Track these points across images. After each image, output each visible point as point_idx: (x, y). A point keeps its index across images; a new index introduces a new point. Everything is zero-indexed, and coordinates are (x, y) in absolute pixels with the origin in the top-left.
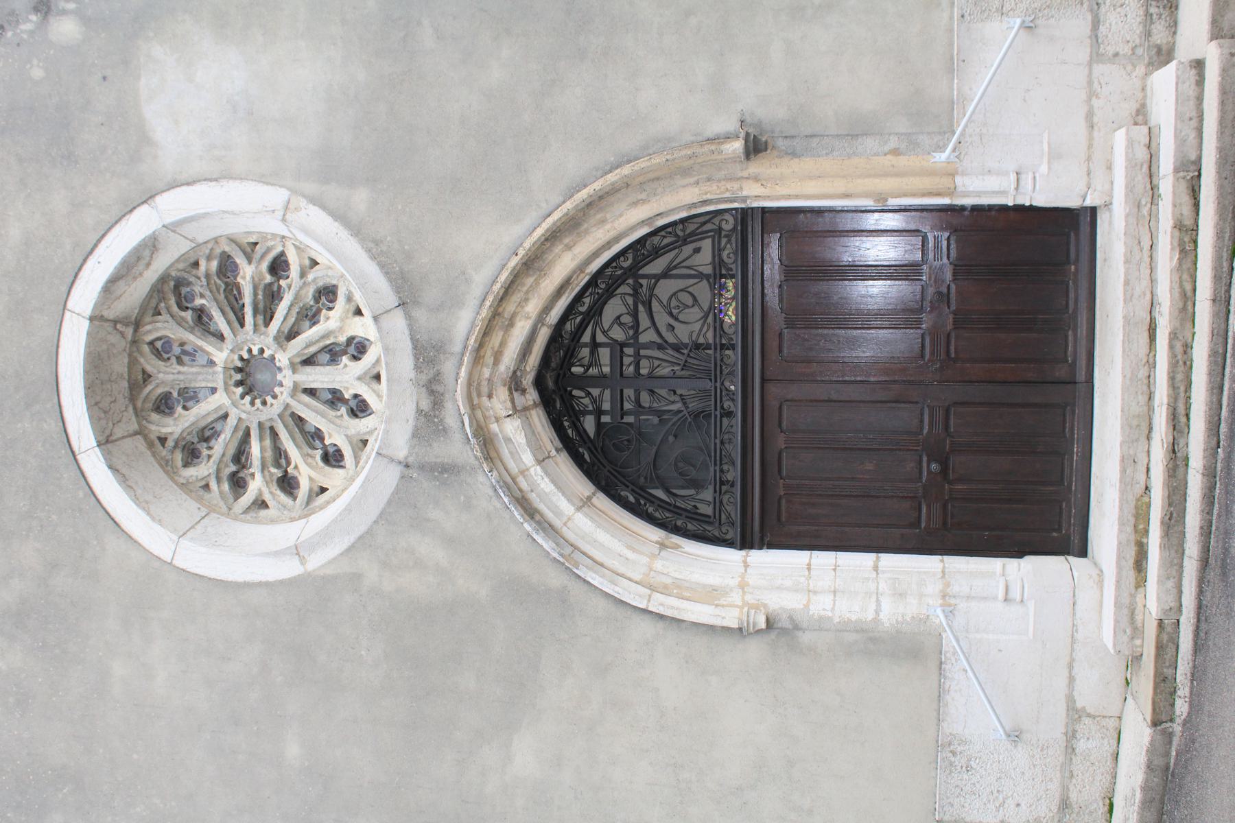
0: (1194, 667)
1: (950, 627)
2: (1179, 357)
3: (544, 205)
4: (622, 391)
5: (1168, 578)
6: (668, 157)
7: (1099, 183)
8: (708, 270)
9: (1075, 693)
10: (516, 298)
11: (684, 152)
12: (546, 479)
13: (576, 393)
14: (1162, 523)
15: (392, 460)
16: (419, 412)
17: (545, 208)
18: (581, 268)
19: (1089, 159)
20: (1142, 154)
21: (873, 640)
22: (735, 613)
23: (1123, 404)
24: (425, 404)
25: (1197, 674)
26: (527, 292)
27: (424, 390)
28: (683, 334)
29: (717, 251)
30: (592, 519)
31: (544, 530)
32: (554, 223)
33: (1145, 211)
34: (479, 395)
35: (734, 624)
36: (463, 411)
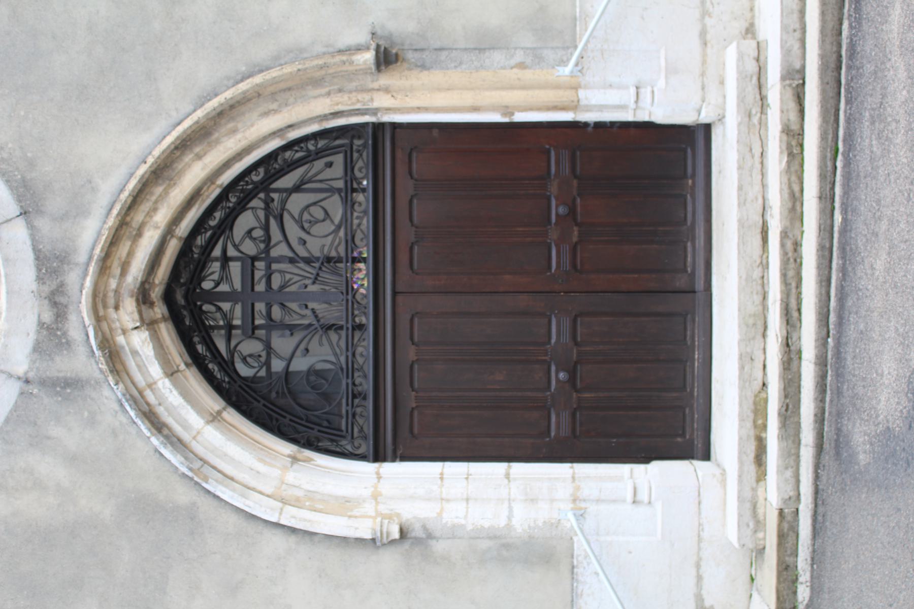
0: (814, 551)
1: (582, 530)
2: (790, 254)
3: (174, 114)
4: (253, 305)
5: (787, 468)
6: (300, 67)
7: (713, 96)
8: (340, 184)
9: (703, 592)
10: (145, 207)
11: (315, 62)
12: (175, 392)
13: (206, 307)
14: (779, 414)
15: (10, 376)
16: (41, 324)
17: (175, 116)
18: (211, 178)
19: (703, 74)
20: (752, 67)
21: (507, 546)
22: (369, 523)
23: (740, 304)
24: (48, 317)
25: (816, 558)
26: (156, 202)
27: (46, 302)
28: (315, 247)
29: (349, 166)
30: (222, 432)
31: (172, 444)
32: (185, 132)
33: (755, 120)
34: (105, 306)
35: (368, 536)
36: (87, 322)
